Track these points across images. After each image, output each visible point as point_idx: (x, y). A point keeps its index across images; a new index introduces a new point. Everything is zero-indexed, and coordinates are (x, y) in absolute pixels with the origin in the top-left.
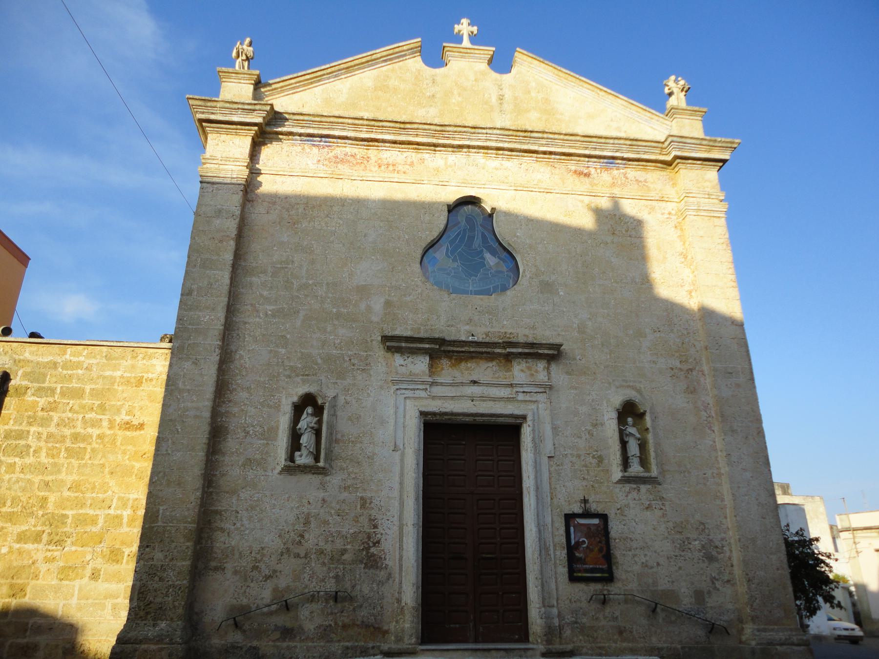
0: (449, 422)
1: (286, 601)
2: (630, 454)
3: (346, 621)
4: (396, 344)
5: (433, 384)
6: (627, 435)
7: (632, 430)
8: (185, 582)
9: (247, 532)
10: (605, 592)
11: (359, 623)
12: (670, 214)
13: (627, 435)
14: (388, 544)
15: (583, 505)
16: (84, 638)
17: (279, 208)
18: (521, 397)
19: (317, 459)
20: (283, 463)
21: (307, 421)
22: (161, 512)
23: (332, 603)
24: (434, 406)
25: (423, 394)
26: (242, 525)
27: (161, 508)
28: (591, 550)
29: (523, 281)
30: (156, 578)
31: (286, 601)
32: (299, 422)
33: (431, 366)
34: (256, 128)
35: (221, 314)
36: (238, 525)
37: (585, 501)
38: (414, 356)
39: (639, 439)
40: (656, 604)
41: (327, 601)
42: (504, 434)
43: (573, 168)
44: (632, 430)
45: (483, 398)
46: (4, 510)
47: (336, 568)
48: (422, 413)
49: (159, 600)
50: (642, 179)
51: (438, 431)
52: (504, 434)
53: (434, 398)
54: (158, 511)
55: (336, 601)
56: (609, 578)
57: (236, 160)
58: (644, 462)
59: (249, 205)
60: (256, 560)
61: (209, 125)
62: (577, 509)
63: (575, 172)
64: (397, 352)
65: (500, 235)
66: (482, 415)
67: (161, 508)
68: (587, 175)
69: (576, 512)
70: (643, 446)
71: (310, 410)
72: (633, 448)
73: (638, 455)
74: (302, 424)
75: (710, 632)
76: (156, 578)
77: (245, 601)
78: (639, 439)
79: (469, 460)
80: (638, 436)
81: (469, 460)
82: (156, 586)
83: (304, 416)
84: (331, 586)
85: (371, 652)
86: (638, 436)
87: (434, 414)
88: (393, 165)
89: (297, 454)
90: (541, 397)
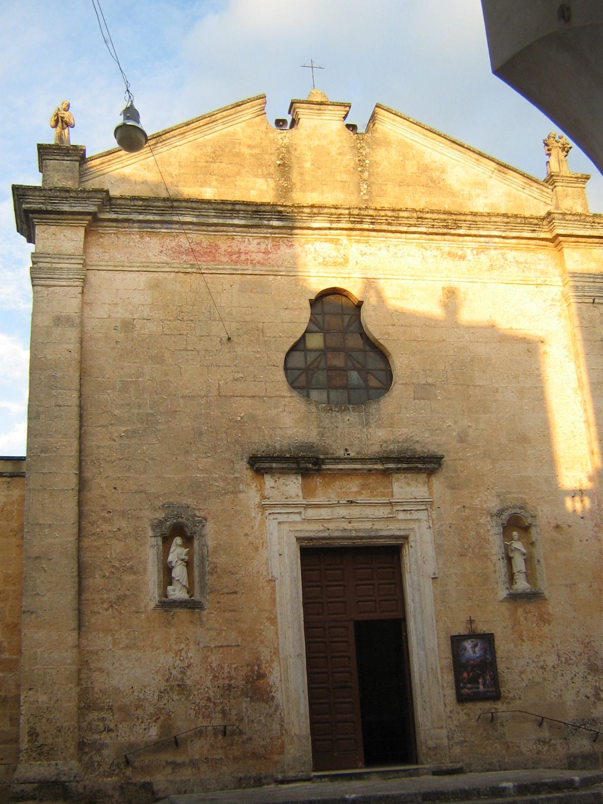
0: (326, 546)
1: (175, 737)
2: (515, 571)
3: (237, 753)
4: (262, 464)
5: (307, 506)
6: (512, 551)
7: (518, 545)
8: (73, 723)
9: (126, 672)
10: (493, 711)
11: (249, 755)
12: (553, 300)
13: (512, 551)
14: (275, 677)
15: (469, 626)
16: (479, 629)
17: (121, 310)
18: (401, 516)
19: (190, 591)
20: (158, 599)
21: (177, 552)
22: (39, 654)
23: (220, 737)
24: (312, 530)
25: (297, 518)
26: (121, 665)
27: (38, 650)
28: (477, 672)
29: (397, 388)
30: (44, 720)
31: (175, 737)
32: (168, 555)
33: (304, 487)
34: (89, 217)
35: (75, 443)
36: (116, 665)
37: (471, 621)
38: (286, 477)
39: (524, 555)
40: (543, 718)
41: (215, 735)
42: (386, 556)
43: (447, 249)
44: (518, 545)
45: (360, 519)
46: (3, 656)
47: (222, 703)
48: (298, 539)
49: (50, 741)
50: (522, 260)
51: (316, 556)
52: (386, 556)
53: (309, 521)
54: (36, 653)
55: (225, 734)
56: (496, 696)
57: (70, 257)
58: (530, 576)
59: (87, 309)
60: (139, 699)
61: (36, 216)
62: (461, 630)
63: (449, 254)
64: (267, 473)
65: (364, 319)
66: (361, 538)
67: (38, 650)
68: (462, 257)
69: (462, 633)
70: (529, 560)
71: (178, 540)
72: (519, 564)
73: (524, 570)
74: (172, 557)
75: (594, 741)
76: (44, 720)
77: (133, 739)
78: (524, 555)
79: (353, 584)
80: (524, 550)
81: (353, 584)
82: (44, 728)
83: (173, 548)
84: (218, 721)
85: (264, 781)
86: (524, 550)
87: (310, 539)
88: (246, 253)
89: (169, 588)
90: (423, 515)
